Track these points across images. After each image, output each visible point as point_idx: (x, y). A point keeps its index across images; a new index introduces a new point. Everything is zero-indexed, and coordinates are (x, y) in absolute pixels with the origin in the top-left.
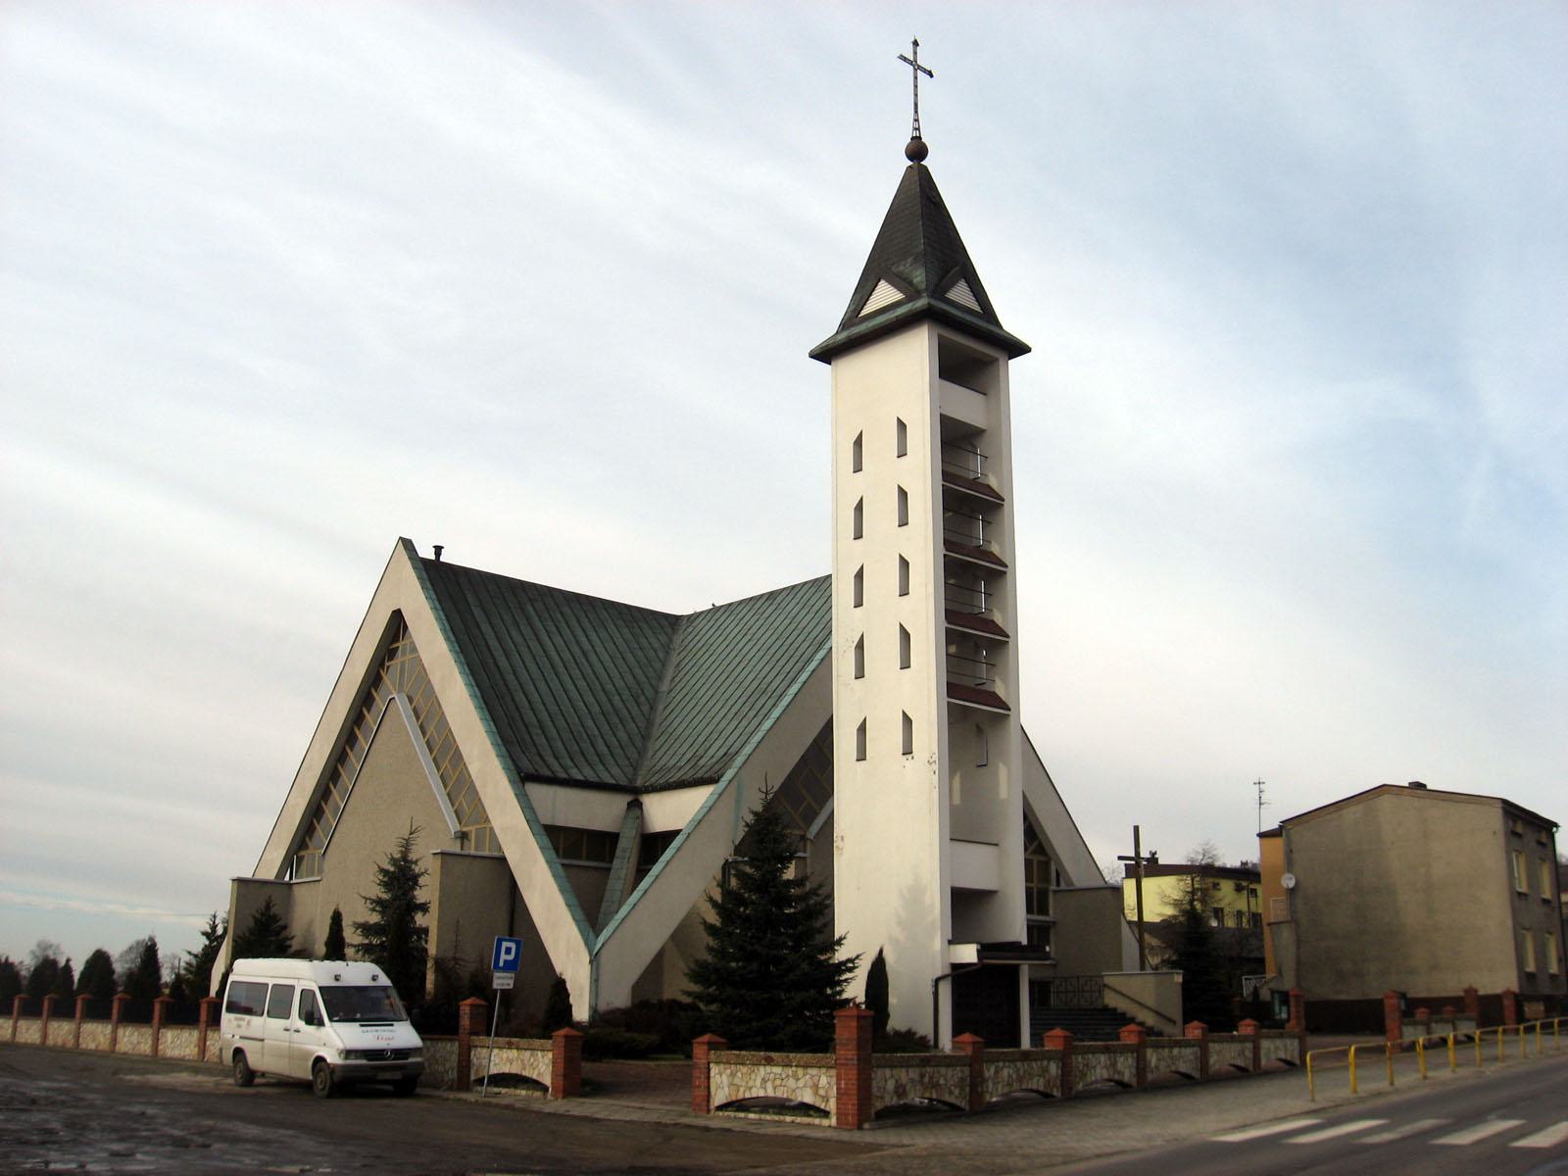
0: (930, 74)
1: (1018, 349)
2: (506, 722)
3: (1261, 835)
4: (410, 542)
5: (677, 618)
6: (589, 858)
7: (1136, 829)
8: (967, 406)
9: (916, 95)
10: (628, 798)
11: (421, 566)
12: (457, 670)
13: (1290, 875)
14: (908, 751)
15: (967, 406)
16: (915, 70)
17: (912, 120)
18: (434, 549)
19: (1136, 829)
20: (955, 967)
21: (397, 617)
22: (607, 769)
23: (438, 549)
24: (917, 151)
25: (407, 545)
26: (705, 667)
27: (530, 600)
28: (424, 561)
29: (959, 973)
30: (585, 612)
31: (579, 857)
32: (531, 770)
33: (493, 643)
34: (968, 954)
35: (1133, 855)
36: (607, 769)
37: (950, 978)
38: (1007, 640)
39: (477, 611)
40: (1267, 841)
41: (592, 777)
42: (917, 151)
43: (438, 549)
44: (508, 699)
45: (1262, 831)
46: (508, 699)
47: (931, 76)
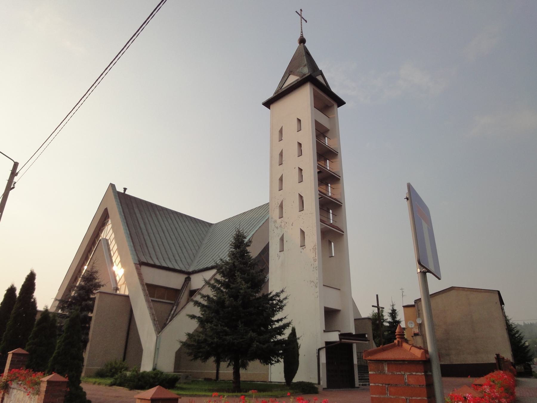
0: (306, 22)
1: (340, 103)
2: (139, 244)
3: (404, 307)
4: (114, 185)
5: (212, 224)
6: (167, 299)
7: (377, 296)
8: (323, 120)
9: (302, 25)
10: (186, 276)
11: (117, 195)
12: (121, 225)
13: (420, 319)
14: (303, 245)
15: (323, 120)
16: (301, 18)
17: (300, 32)
18: (123, 189)
19: (377, 296)
20: (327, 343)
21: (106, 210)
22: (178, 265)
23: (125, 189)
24: (302, 41)
25: (112, 186)
26: (222, 248)
27: (158, 210)
28: (119, 193)
29: (330, 346)
30: (178, 217)
31: (164, 299)
32: (145, 261)
33: (142, 226)
34: (334, 337)
35: (376, 305)
36: (178, 265)
37: (325, 349)
38: (341, 204)
39: (138, 215)
40: (406, 309)
41: (171, 266)
42: (302, 41)
43: (125, 189)
44: (142, 238)
45: (404, 305)
46: (142, 238)
47: (306, 22)
